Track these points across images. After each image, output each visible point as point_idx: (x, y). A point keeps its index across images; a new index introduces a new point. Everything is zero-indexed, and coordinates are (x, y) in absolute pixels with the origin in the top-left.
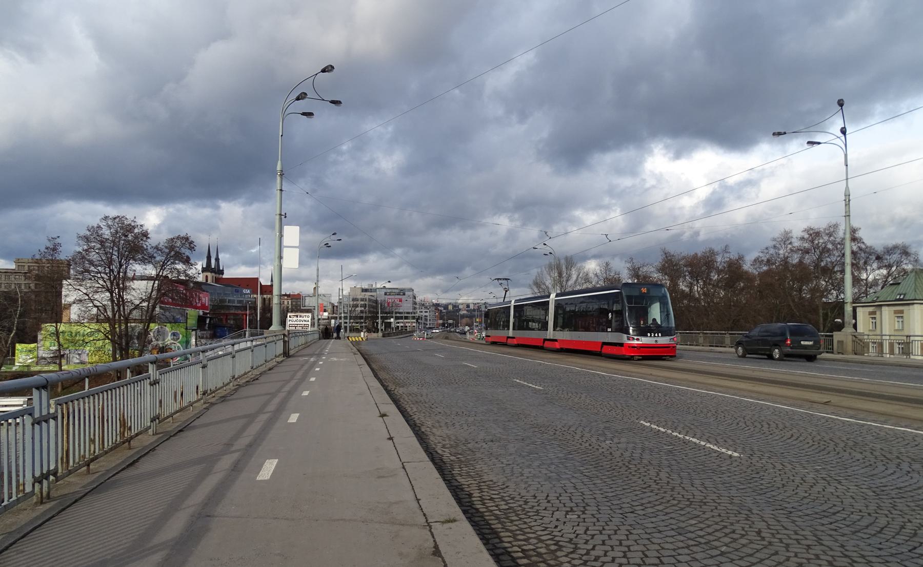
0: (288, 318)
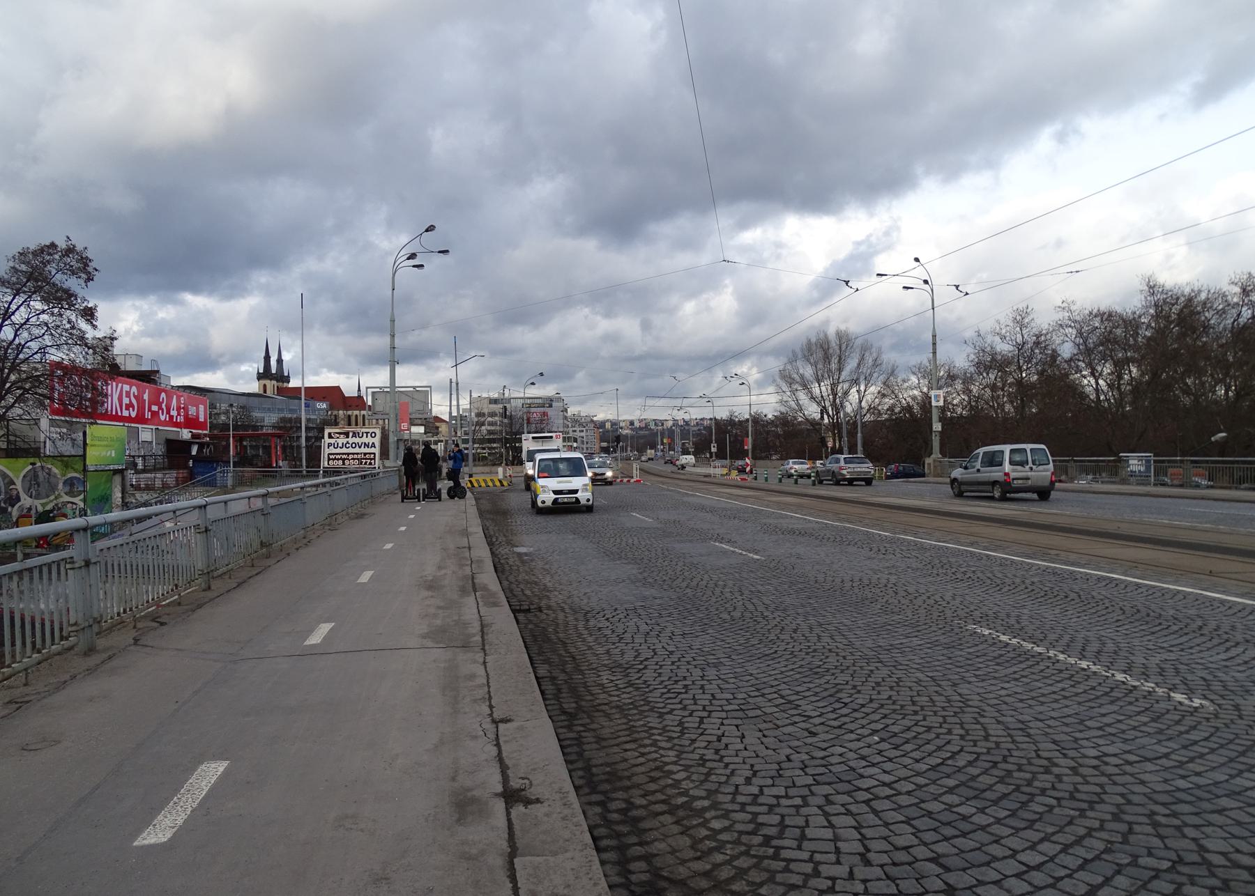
0: (327, 440)
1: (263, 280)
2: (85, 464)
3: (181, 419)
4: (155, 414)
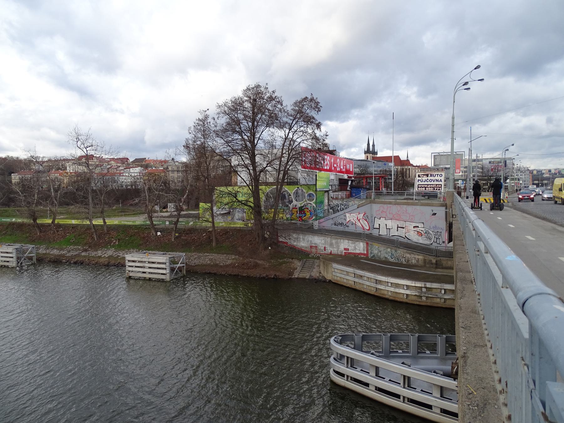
0: (417, 178)
1: (356, 113)
2: (316, 188)
3: (344, 170)
4: (336, 168)
